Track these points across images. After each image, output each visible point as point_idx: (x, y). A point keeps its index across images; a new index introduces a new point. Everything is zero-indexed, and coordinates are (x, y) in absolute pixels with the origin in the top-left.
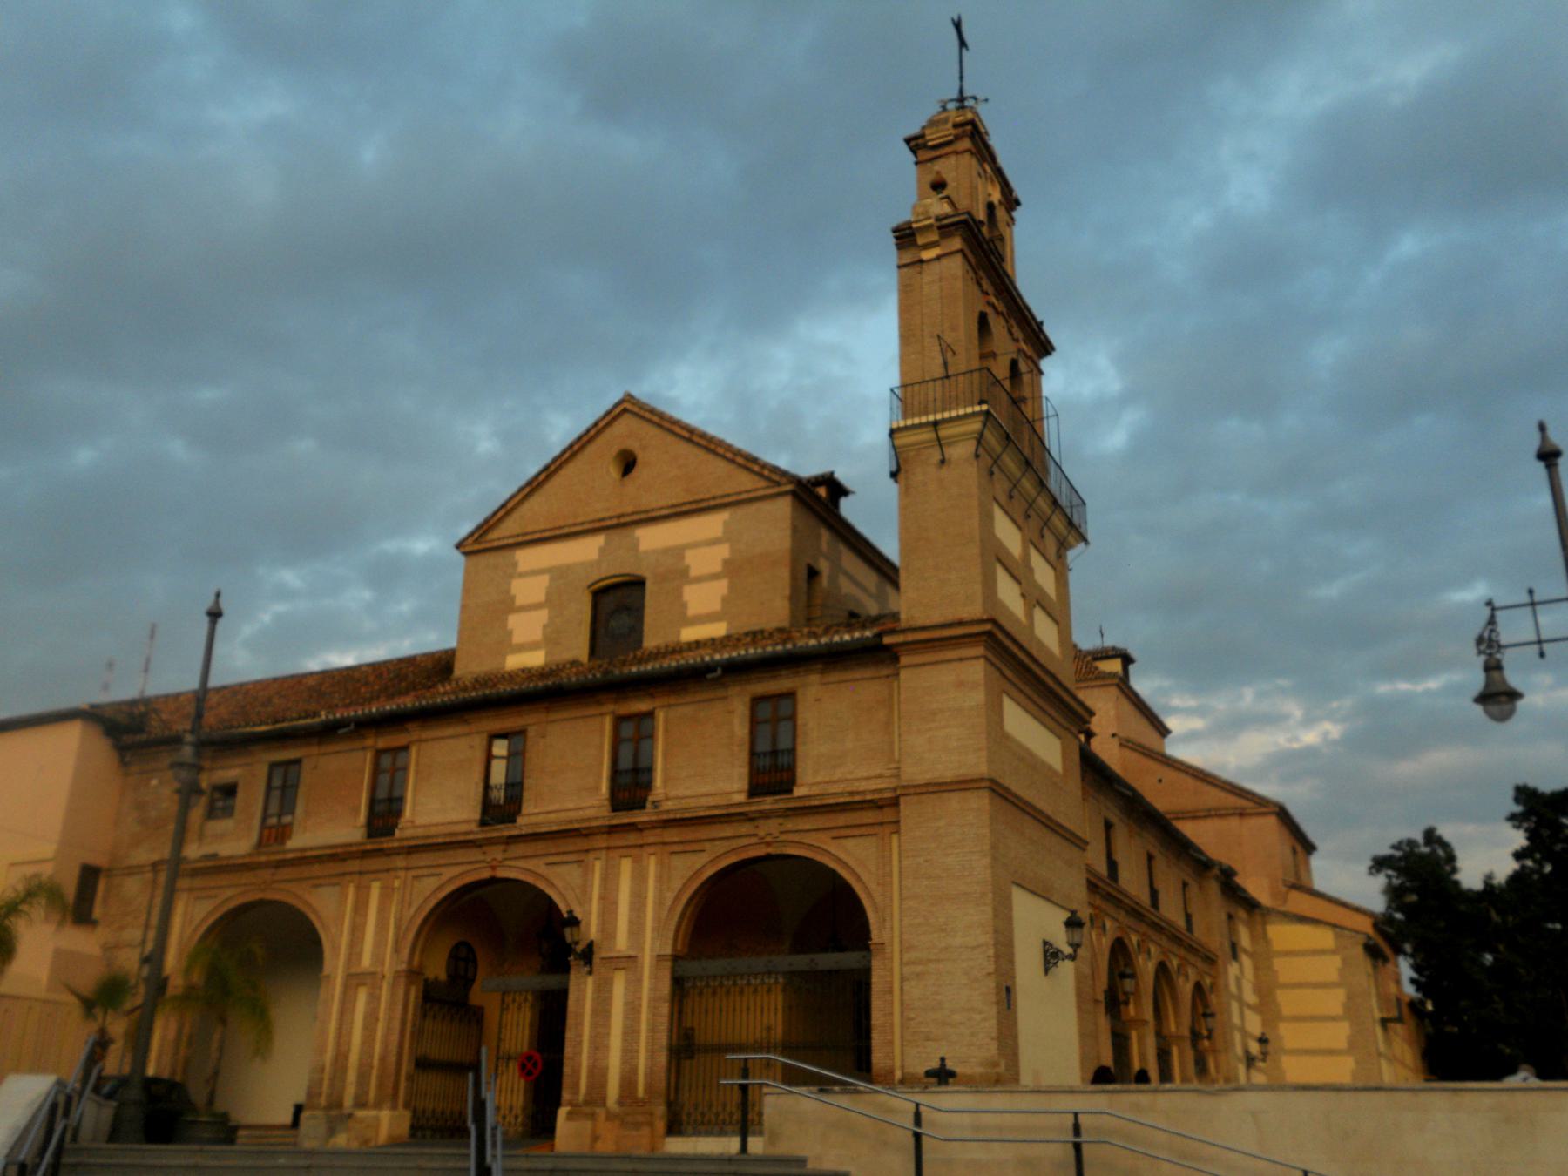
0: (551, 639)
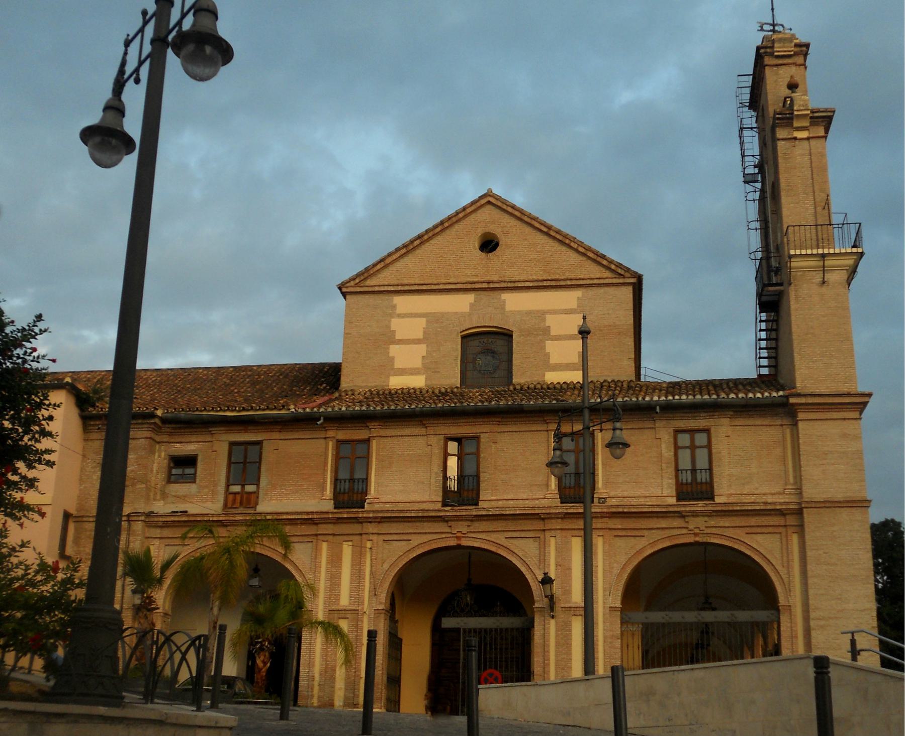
0: (428, 367)
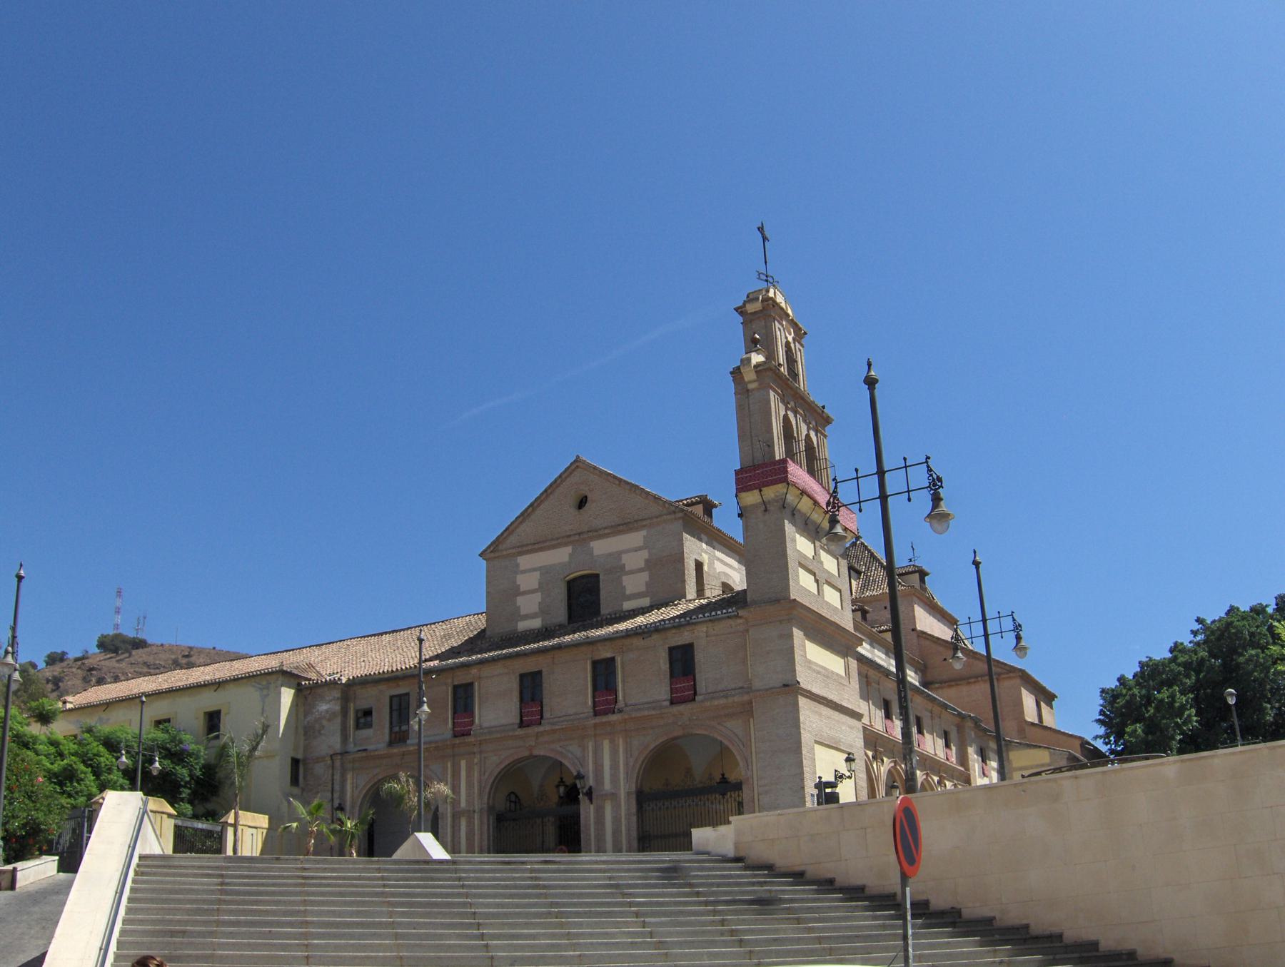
0: (544, 611)
